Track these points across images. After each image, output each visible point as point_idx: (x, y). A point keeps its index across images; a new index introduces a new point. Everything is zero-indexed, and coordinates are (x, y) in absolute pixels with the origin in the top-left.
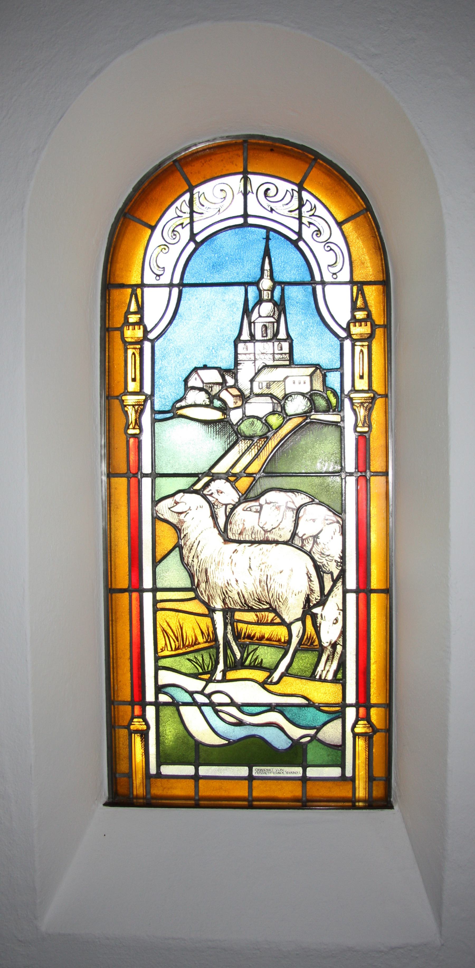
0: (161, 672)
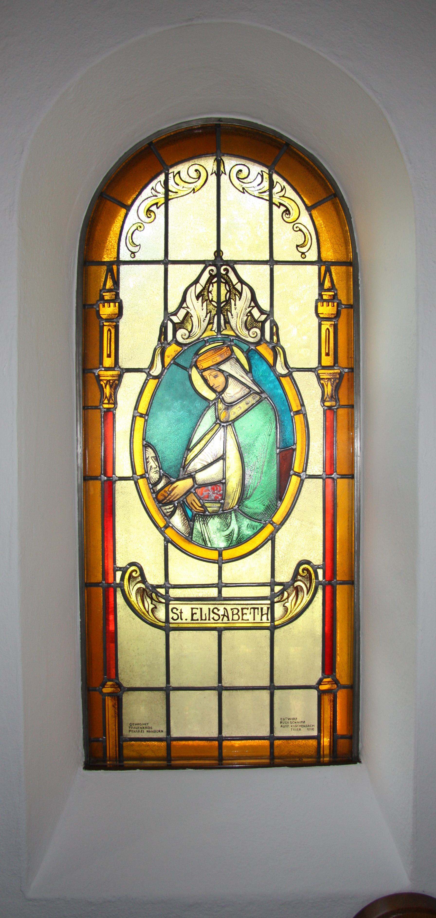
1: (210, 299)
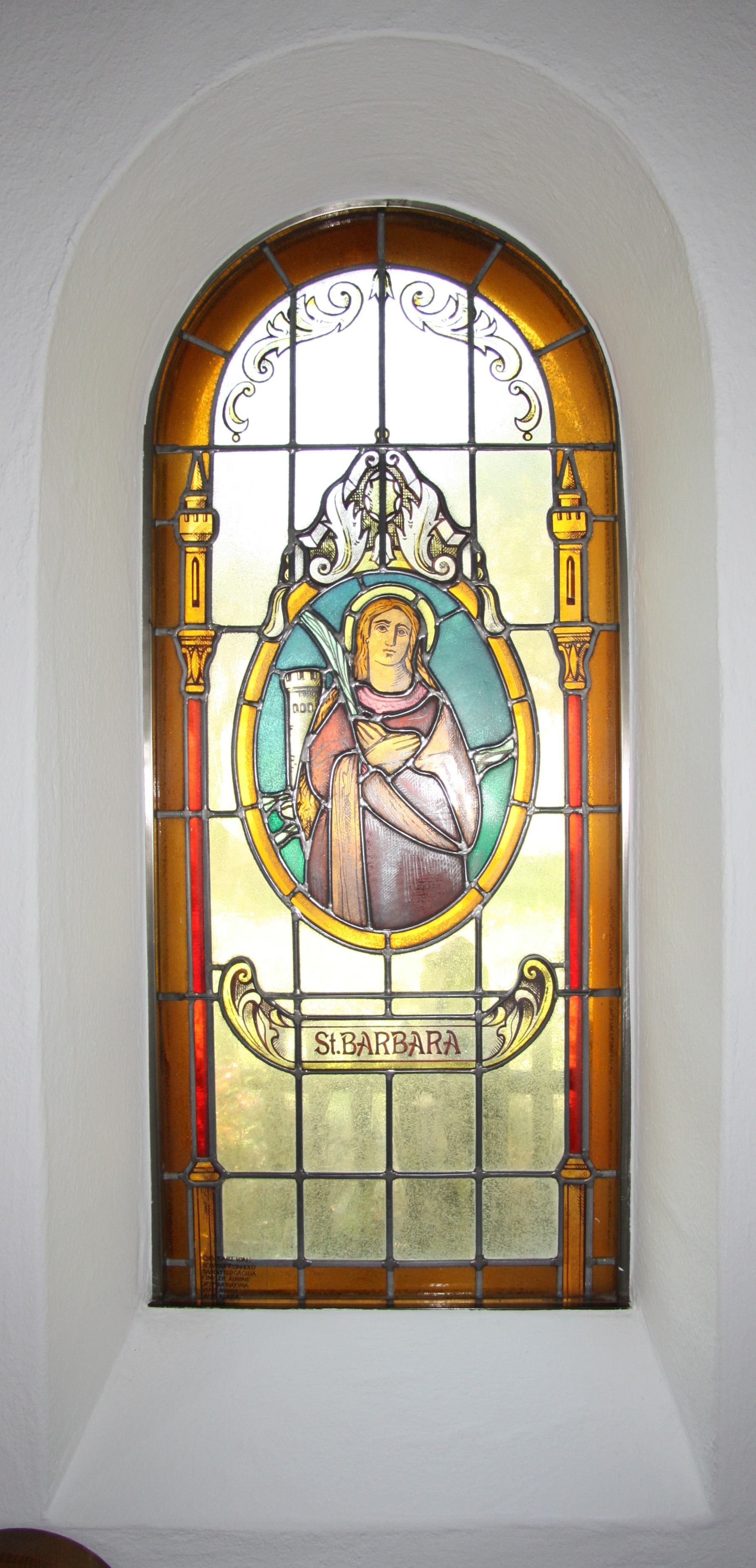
1: (368, 508)
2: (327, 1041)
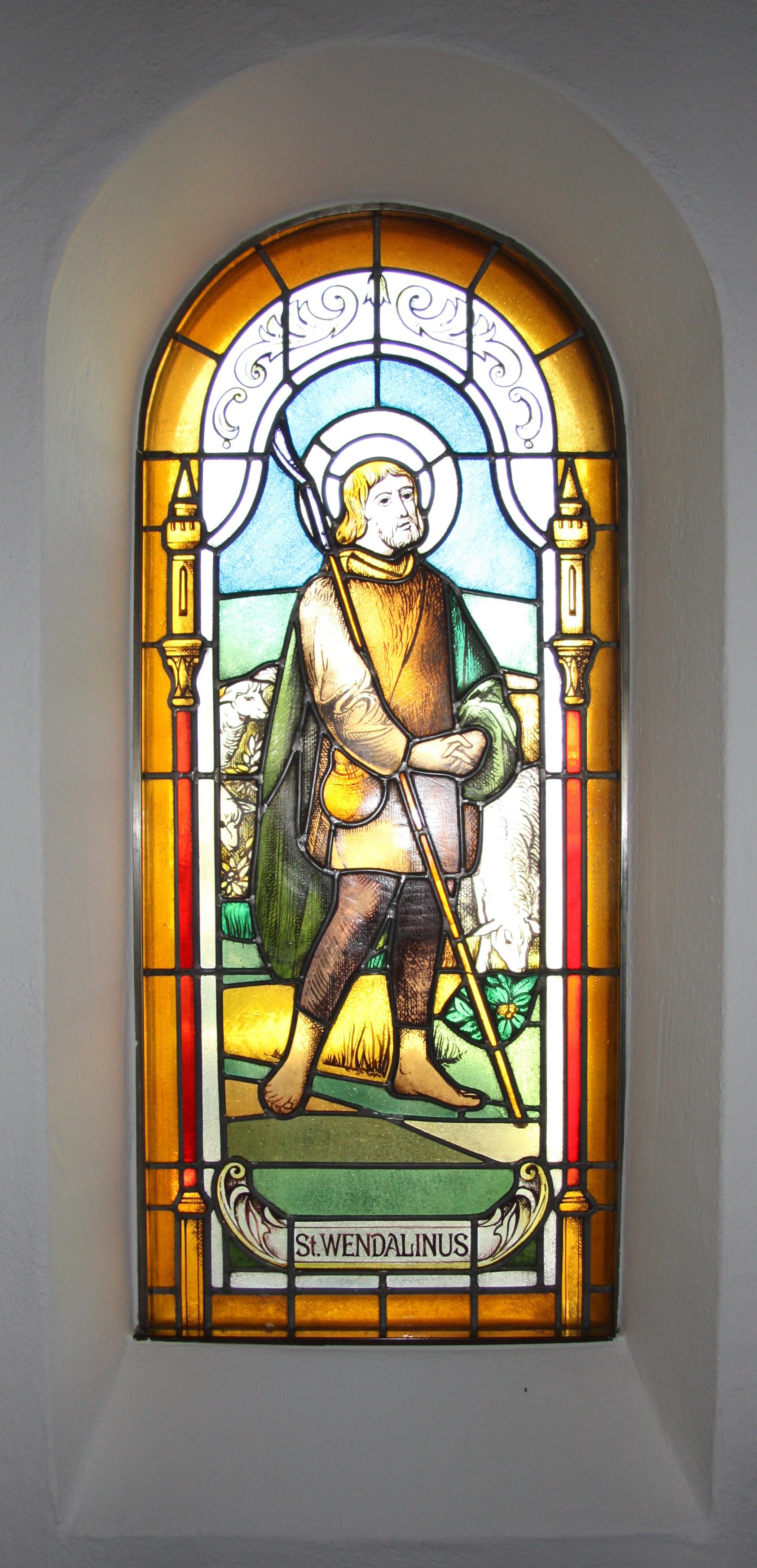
0: (227, 1082)
2: (308, 1243)
